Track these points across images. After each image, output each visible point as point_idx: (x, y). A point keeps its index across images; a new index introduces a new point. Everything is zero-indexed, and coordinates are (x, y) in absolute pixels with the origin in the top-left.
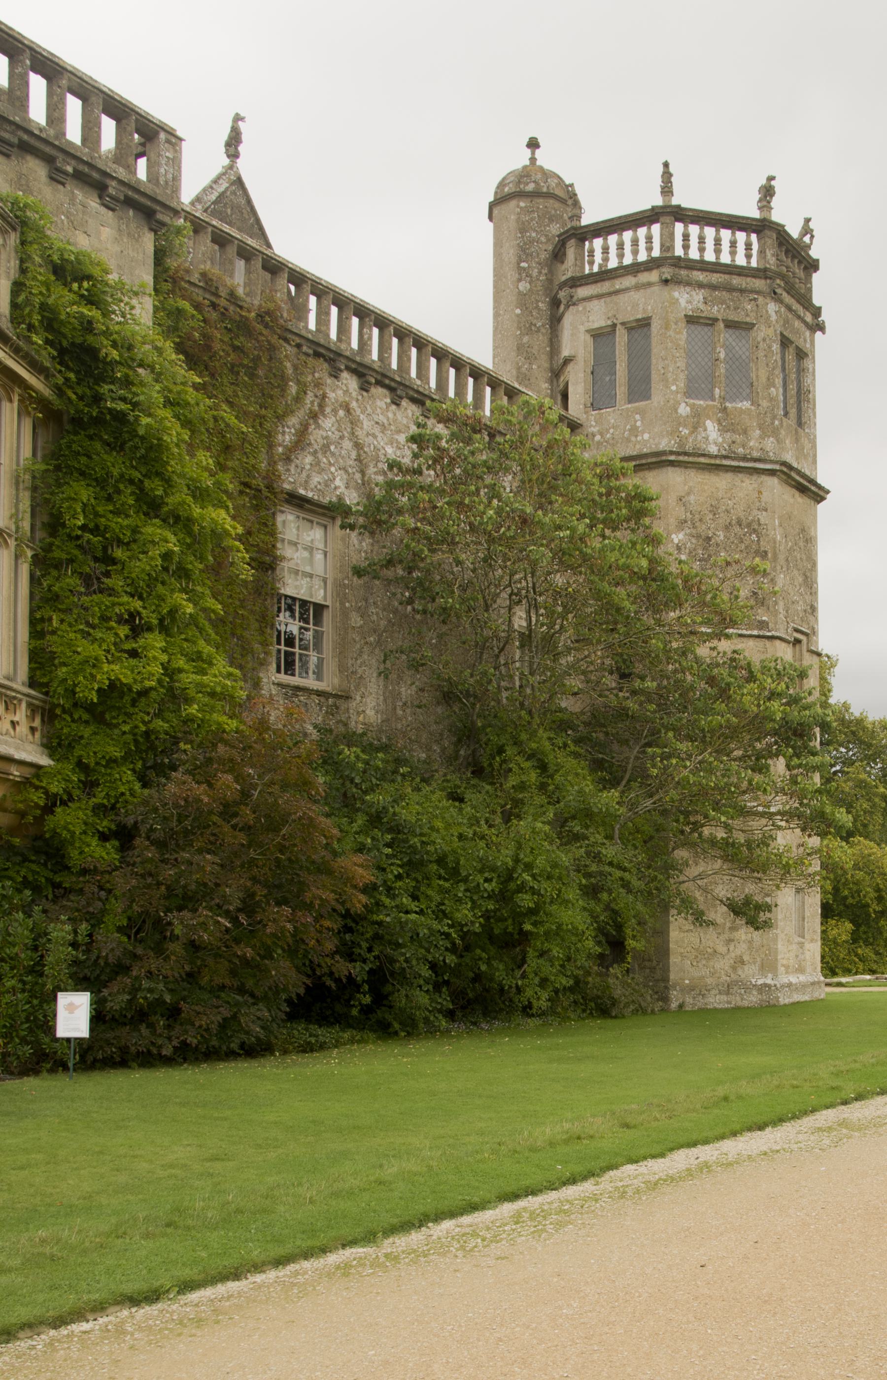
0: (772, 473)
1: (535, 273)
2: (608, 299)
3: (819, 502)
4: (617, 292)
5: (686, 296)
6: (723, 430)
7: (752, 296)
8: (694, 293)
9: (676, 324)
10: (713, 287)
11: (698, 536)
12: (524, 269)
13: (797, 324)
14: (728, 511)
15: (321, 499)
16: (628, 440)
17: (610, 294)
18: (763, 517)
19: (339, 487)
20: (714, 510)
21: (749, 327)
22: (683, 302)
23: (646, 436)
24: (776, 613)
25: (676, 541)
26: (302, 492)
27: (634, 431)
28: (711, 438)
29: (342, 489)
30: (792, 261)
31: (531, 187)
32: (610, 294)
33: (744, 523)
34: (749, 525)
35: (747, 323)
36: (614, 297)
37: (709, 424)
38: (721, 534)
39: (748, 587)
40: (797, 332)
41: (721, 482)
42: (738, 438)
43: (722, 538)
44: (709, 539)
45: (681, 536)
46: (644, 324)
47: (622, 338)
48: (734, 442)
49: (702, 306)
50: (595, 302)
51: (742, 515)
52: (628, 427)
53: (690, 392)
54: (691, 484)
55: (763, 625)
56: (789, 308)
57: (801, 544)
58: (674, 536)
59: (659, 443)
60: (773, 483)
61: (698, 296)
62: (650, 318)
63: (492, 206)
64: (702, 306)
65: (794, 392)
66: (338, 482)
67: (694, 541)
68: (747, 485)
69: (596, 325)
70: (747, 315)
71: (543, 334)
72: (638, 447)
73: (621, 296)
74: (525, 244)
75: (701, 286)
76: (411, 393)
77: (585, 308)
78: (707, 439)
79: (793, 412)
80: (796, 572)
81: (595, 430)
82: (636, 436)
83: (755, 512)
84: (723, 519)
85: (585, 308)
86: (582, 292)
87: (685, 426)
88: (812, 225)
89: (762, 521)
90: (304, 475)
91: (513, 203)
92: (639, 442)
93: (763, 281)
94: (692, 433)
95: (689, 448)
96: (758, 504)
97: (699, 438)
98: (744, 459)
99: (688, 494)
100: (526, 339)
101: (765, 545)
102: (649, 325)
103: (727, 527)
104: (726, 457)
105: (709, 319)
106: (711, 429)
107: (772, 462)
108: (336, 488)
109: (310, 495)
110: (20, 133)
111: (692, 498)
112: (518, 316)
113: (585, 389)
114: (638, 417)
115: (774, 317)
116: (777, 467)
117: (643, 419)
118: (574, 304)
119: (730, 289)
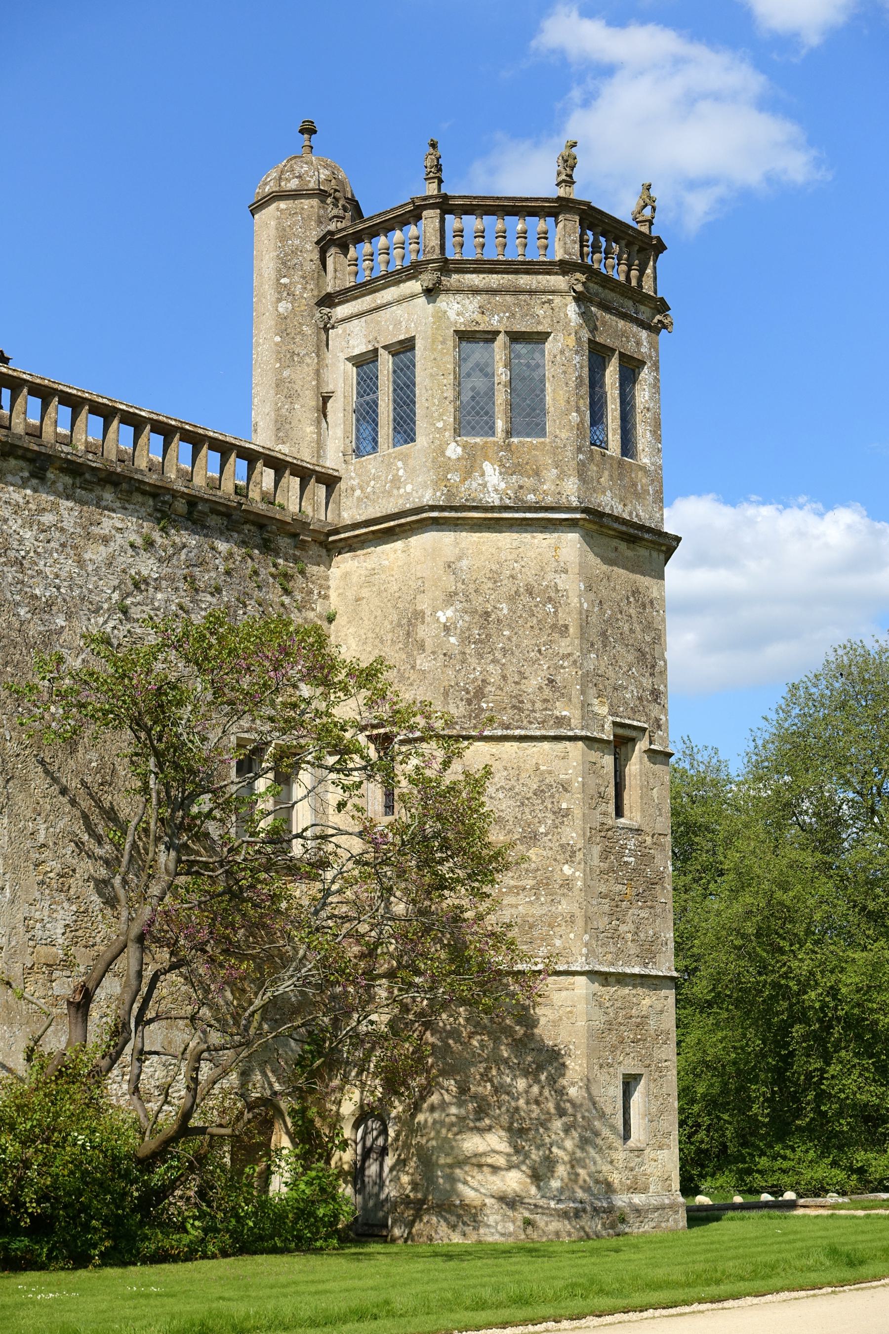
0: (571, 525)
5: (456, 306)
6: (506, 472)
7: (545, 298)
8: (467, 301)
12: (285, 285)
14: (512, 577)
18: (562, 582)
21: (542, 337)
23: (409, 488)
25: (443, 620)
27: (396, 482)
35: (538, 333)
36: (375, 315)
37: (487, 467)
38: (505, 608)
42: (528, 482)
43: (505, 611)
44: (487, 614)
45: (450, 613)
46: (405, 347)
47: (386, 363)
48: (521, 487)
49: (477, 316)
50: (356, 322)
52: (390, 477)
54: (463, 545)
55: (560, 721)
58: (440, 614)
59: (423, 496)
61: (472, 304)
62: (412, 340)
64: (477, 316)
67: (467, 618)
68: (540, 541)
69: (357, 352)
70: (539, 323)
71: (308, 365)
72: (400, 502)
74: (286, 255)
75: (476, 291)
77: (344, 331)
78: (484, 485)
81: (355, 482)
82: (399, 488)
84: (508, 587)
86: (342, 311)
88: (653, 193)
89: (561, 586)
92: (401, 496)
99: (460, 558)
101: (564, 617)
102: (413, 348)
103: (512, 599)
104: (507, 508)
111: (464, 563)
112: (277, 344)
113: (345, 432)
118: (333, 327)
119: (517, 291)
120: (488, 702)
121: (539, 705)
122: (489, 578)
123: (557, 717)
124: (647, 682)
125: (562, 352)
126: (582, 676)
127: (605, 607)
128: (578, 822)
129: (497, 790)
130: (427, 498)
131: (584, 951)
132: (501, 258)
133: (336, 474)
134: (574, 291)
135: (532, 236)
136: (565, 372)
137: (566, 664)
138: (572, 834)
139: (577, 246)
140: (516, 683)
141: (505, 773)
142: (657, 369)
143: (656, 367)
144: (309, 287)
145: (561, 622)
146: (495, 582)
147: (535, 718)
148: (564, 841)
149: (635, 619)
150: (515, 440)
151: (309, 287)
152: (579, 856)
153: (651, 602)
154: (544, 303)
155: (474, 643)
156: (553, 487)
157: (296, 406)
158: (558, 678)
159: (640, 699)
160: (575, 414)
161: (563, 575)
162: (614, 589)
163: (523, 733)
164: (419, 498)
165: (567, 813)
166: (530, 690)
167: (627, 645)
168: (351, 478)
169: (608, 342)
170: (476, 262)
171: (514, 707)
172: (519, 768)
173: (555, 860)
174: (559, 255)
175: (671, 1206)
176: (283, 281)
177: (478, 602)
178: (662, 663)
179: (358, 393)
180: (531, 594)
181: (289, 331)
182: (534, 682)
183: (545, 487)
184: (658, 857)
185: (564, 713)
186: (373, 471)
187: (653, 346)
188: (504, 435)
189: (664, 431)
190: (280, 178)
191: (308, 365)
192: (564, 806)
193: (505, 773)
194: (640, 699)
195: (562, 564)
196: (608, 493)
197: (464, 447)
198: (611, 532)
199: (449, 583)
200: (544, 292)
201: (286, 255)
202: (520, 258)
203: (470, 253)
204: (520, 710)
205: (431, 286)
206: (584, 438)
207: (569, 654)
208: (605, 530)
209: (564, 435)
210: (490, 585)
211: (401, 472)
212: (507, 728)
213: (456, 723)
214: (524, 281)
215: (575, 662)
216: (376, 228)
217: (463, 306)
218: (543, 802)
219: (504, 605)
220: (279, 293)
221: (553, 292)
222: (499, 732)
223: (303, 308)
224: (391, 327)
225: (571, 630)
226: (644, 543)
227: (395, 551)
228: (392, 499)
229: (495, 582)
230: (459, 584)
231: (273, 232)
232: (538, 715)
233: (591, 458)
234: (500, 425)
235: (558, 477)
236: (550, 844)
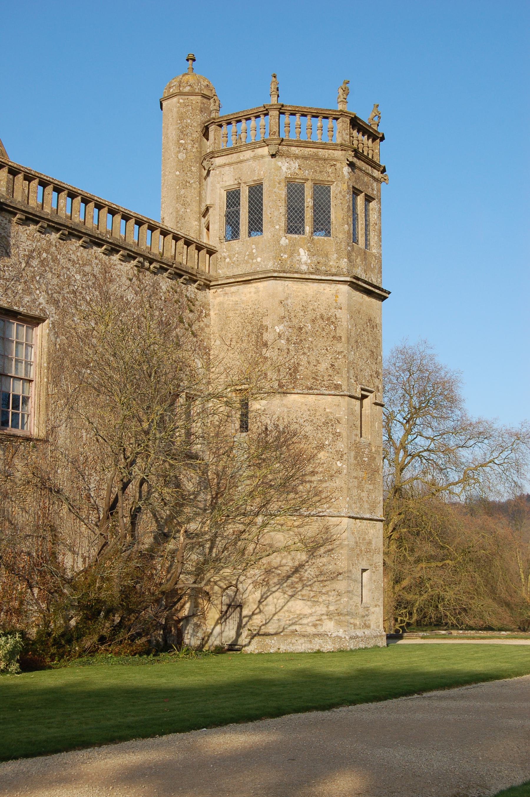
1: (189, 147)
2: (235, 166)
3: (383, 301)
4: (241, 162)
6: (311, 254)
8: (292, 162)
9: (279, 184)
10: (305, 158)
12: (182, 144)
13: (366, 179)
15: (29, 312)
16: (247, 262)
19: (42, 304)
20: (304, 309)
22: (284, 169)
23: (259, 260)
25: (278, 331)
26: (16, 308)
27: (252, 256)
28: (303, 260)
29: (44, 304)
30: (363, 135)
31: (187, 89)
33: (326, 317)
34: (328, 319)
37: (301, 251)
38: (309, 326)
40: (366, 185)
41: (311, 288)
42: (321, 259)
43: (310, 328)
44: (301, 329)
48: (319, 263)
49: (297, 171)
50: (227, 168)
51: (323, 312)
52: (247, 253)
57: (368, 330)
58: (276, 327)
61: (295, 165)
66: (41, 300)
70: (329, 176)
71: (195, 189)
72: (254, 266)
73: (243, 164)
74: (183, 127)
75: (297, 157)
77: (220, 172)
80: (364, 350)
82: (253, 260)
83: (333, 310)
84: (310, 315)
85: (220, 172)
86: (218, 161)
90: (17, 297)
91: (175, 99)
92: (254, 263)
93: (340, 152)
95: (287, 267)
96: (335, 304)
97: (295, 260)
98: (326, 273)
99: (287, 299)
100: (183, 191)
105: (303, 179)
106: (303, 255)
107: (344, 275)
108: (40, 304)
109: (21, 309)
111: (289, 301)
112: (177, 176)
113: (220, 227)
114: (254, 246)
117: (257, 248)
119: (316, 158)
120: (300, 375)
121: (326, 378)
122: (302, 310)
123: (335, 385)
124: (374, 367)
125: (340, 192)
126: (348, 364)
127: (357, 327)
128: (345, 439)
129: (305, 421)
130: (270, 265)
131: (347, 506)
132: (309, 140)
133: (215, 249)
134: (348, 160)
135: (325, 130)
136: (342, 203)
137: (340, 357)
138: (341, 445)
139: (348, 136)
140: (315, 366)
141: (309, 413)
142: (380, 203)
143: (379, 202)
144: (195, 146)
145: (338, 335)
146: (305, 312)
147: (324, 384)
148: (338, 449)
149: (369, 334)
150: (316, 237)
151: (195, 146)
152: (345, 457)
153: (376, 326)
154: (331, 166)
155: (294, 344)
156: (335, 264)
157: (188, 210)
158: (336, 364)
159: (371, 376)
160: (346, 226)
161: (339, 310)
162: (361, 319)
163: (318, 392)
164: (265, 265)
165: (339, 434)
166: (322, 370)
167: (366, 348)
168: (224, 252)
169: (360, 188)
170: (297, 141)
171: (313, 378)
172: (316, 410)
173: (333, 459)
174: (339, 141)
175: (380, 636)
176: (182, 141)
177: (295, 321)
178: (380, 357)
179: (227, 206)
180: (323, 319)
181: (184, 169)
182: (323, 366)
183: (331, 264)
184: (377, 458)
185: (339, 383)
186: (237, 249)
187: (379, 191)
188: (310, 234)
189: (382, 236)
190: (180, 86)
191: (195, 189)
192: (338, 431)
193: (309, 413)
194: (371, 376)
195: (339, 304)
196: (360, 268)
197: (289, 240)
198: (361, 289)
199: (281, 311)
200: (332, 160)
201: (183, 127)
202: (319, 141)
203: (293, 137)
204: (317, 380)
205: (274, 153)
206: (350, 239)
207: (342, 352)
208: (359, 287)
209: (341, 236)
210: (302, 313)
211: (254, 251)
212: (310, 389)
213: (284, 385)
214: (322, 152)
215: (345, 356)
216: (241, 118)
217: (290, 164)
218: (328, 428)
219: (309, 324)
220: (179, 148)
221: (336, 160)
222: (306, 391)
223: (192, 157)
224: (249, 173)
225: (343, 339)
226: (375, 294)
227: (250, 293)
228: (249, 265)
229: (305, 312)
230: (286, 312)
231: (175, 115)
232: (325, 383)
233: (353, 249)
234: (308, 229)
235: (337, 258)
236: (330, 450)
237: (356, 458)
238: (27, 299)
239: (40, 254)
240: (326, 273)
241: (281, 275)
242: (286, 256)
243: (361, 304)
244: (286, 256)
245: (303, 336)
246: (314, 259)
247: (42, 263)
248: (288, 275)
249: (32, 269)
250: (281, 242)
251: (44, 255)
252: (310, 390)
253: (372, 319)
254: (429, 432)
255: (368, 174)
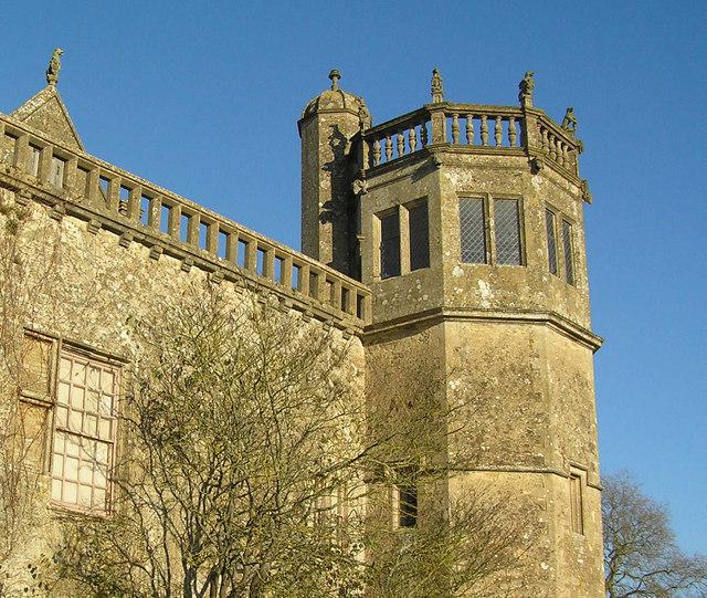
4: (398, 179)
6: (495, 287)
8: (463, 173)
10: (481, 167)
11: (475, 382)
17: (392, 181)
18: (535, 363)
20: (488, 358)
22: (454, 181)
24: (551, 450)
25: (453, 387)
27: (416, 294)
32: (392, 181)
34: (522, 371)
37: (481, 283)
39: (523, 427)
40: (563, 202)
42: (510, 294)
45: (458, 383)
51: (515, 361)
53: (466, 258)
55: (538, 461)
56: (553, 181)
57: (576, 388)
60: (545, 330)
61: (467, 176)
63: (300, 123)
65: (563, 254)
66: (124, 335)
75: (470, 167)
76: (200, 261)
77: (372, 196)
79: (562, 270)
80: (571, 412)
87: (460, 287)
90: (90, 328)
94: (464, 292)
99: (464, 345)
106: (484, 288)
107: (540, 312)
109: (94, 345)
110: (223, 271)
111: (468, 348)
115: (538, 189)
116: (546, 317)
119: (495, 167)
148: (541, 545)
177: (477, 375)
182: (518, 432)
192: (541, 520)
235: (530, 291)
237: (567, 559)
238: (102, 331)
239: (123, 276)
240: (515, 310)
241: (455, 313)
242: (461, 290)
243: (565, 353)
244: (461, 290)
245: (488, 394)
246: (499, 292)
247: (128, 287)
248: (465, 314)
249: (111, 293)
250: (454, 273)
251: (130, 277)
252: (499, 466)
253: (581, 373)
254: (635, 572)
255: (564, 189)
